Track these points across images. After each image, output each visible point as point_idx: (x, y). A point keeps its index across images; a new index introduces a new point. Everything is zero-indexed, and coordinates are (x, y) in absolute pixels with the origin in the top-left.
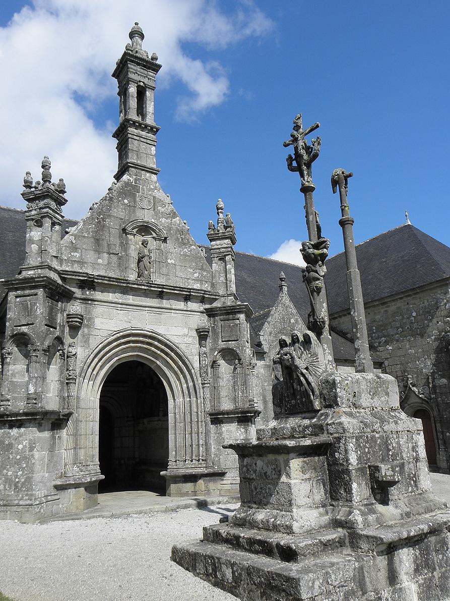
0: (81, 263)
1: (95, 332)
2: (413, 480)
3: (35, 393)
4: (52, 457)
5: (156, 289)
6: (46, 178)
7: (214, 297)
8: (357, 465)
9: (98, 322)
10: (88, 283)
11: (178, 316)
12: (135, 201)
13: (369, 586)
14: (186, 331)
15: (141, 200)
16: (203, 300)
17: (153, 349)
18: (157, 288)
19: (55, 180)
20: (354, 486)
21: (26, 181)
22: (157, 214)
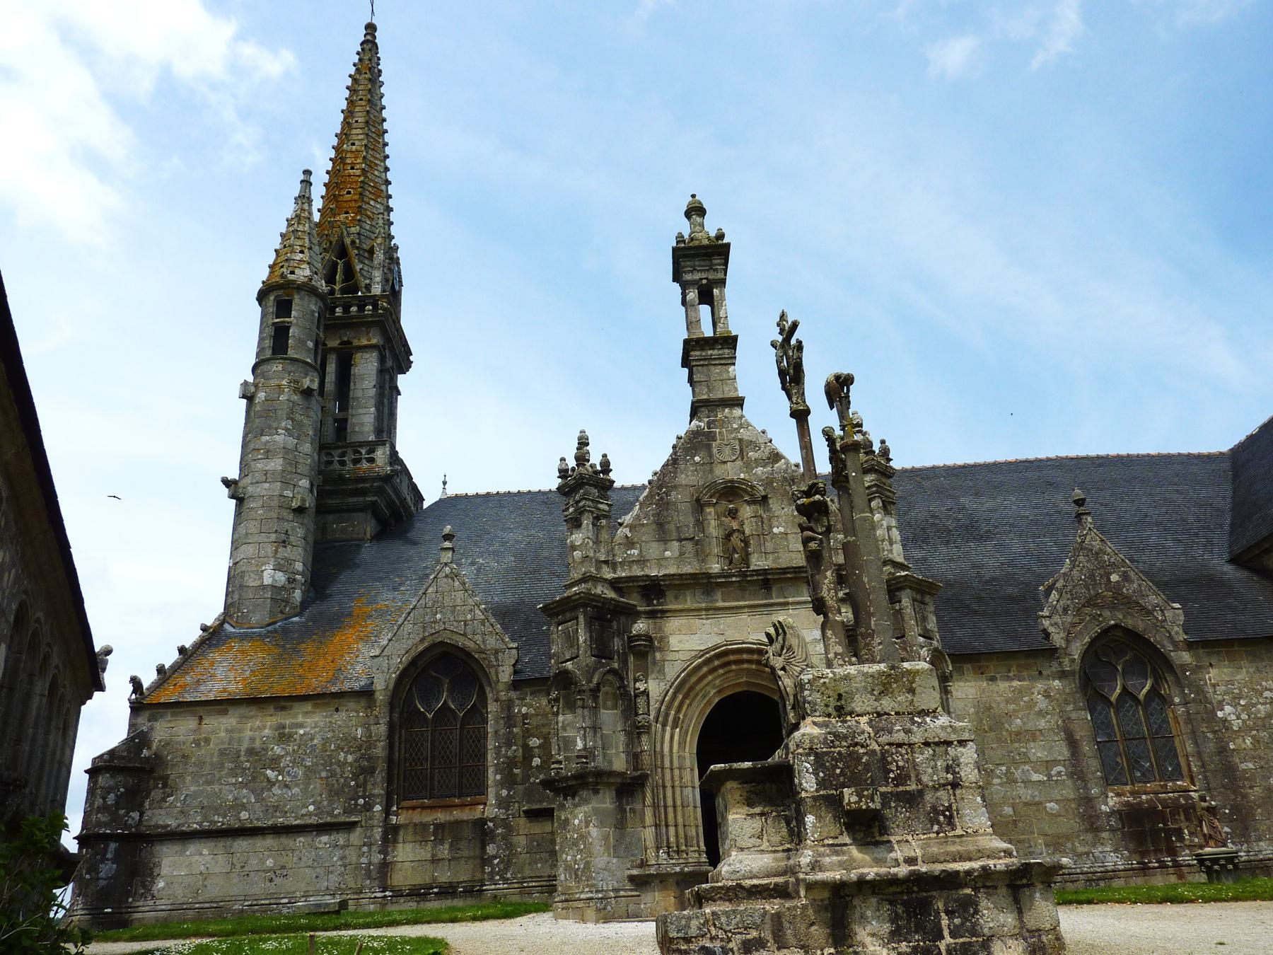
0: (642, 562)
1: (670, 656)
2: (945, 816)
3: (585, 749)
4: (622, 836)
6: (582, 458)
8: (817, 790)
9: (674, 642)
10: (654, 589)
12: (711, 455)
15: (720, 452)
17: (745, 666)
19: (595, 459)
20: (810, 819)
21: (560, 471)
22: (749, 465)
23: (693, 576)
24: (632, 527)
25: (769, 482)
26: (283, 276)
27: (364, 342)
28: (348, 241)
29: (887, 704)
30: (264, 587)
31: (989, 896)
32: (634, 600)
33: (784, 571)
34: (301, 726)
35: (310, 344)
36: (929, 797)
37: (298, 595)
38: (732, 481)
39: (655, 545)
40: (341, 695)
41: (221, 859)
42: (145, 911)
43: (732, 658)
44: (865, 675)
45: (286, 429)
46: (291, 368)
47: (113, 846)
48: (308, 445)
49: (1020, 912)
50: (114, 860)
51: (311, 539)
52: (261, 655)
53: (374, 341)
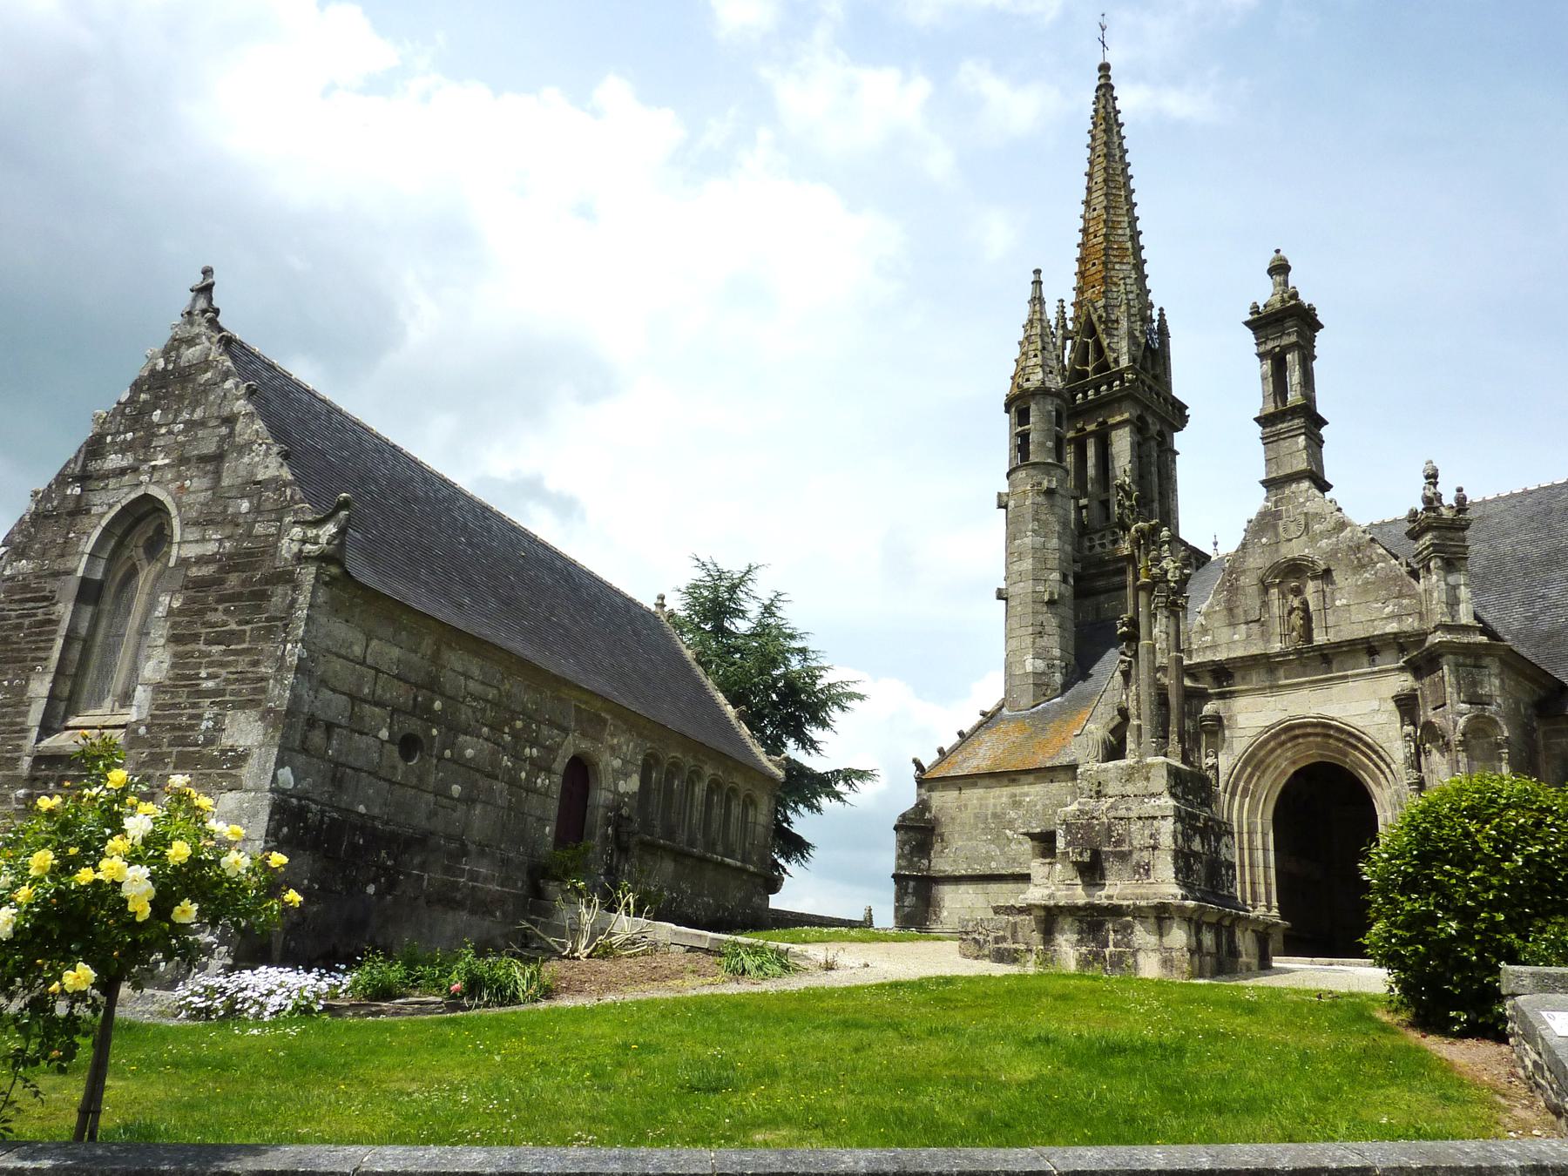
0: (1214, 647)
9: (1241, 720)
10: (1223, 673)
11: (1361, 684)
12: (1277, 535)
13: (1020, 938)
14: (1375, 704)
15: (1285, 530)
16: (1402, 649)
22: (1313, 540)
23: (1254, 657)
24: (1206, 615)
25: (1333, 553)
26: (1019, 386)
27: (1118, 418)
28: (1095, 318)
29: (1130, 789)
30: (1027, 674)
31: (1141, 923)
32: (1206, 684)
33: (1339, 645)
34: (1027, 795)
35: (1050, 444)
36: (1136, 856)
37: (1058, 678)
38: (1293, 559)
39: (1225, 630)
40: (1053, 769)
41: (981, 898)
42: (936, 928)
43: (1297, 732)
44: (1117, 767)
45: (1034, 531)
46: (1032, 472)
47: (912, 884)
48: (1055, 541)
49: (1161, 936)
50: (914, 894)
51: (1070, 625)
52: (1016, 736)
53: (1126, 415)
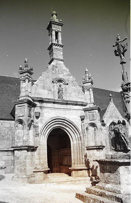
5: (65, 102)
7: (85, 104)
18: (65, 102)
